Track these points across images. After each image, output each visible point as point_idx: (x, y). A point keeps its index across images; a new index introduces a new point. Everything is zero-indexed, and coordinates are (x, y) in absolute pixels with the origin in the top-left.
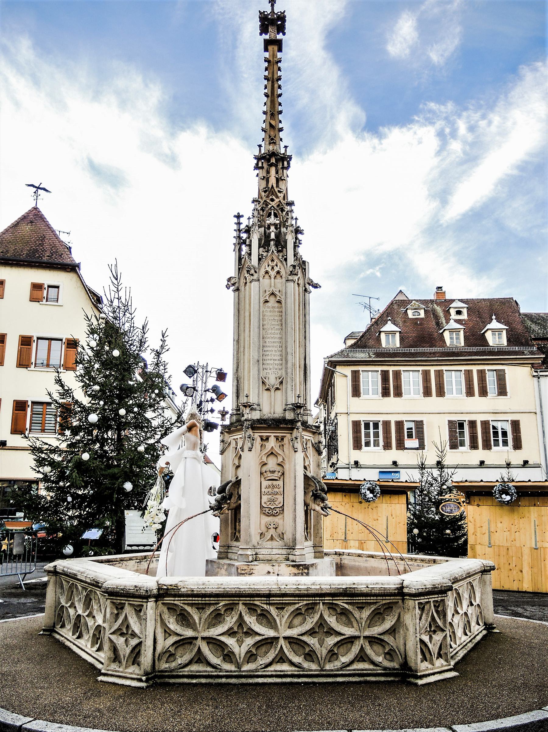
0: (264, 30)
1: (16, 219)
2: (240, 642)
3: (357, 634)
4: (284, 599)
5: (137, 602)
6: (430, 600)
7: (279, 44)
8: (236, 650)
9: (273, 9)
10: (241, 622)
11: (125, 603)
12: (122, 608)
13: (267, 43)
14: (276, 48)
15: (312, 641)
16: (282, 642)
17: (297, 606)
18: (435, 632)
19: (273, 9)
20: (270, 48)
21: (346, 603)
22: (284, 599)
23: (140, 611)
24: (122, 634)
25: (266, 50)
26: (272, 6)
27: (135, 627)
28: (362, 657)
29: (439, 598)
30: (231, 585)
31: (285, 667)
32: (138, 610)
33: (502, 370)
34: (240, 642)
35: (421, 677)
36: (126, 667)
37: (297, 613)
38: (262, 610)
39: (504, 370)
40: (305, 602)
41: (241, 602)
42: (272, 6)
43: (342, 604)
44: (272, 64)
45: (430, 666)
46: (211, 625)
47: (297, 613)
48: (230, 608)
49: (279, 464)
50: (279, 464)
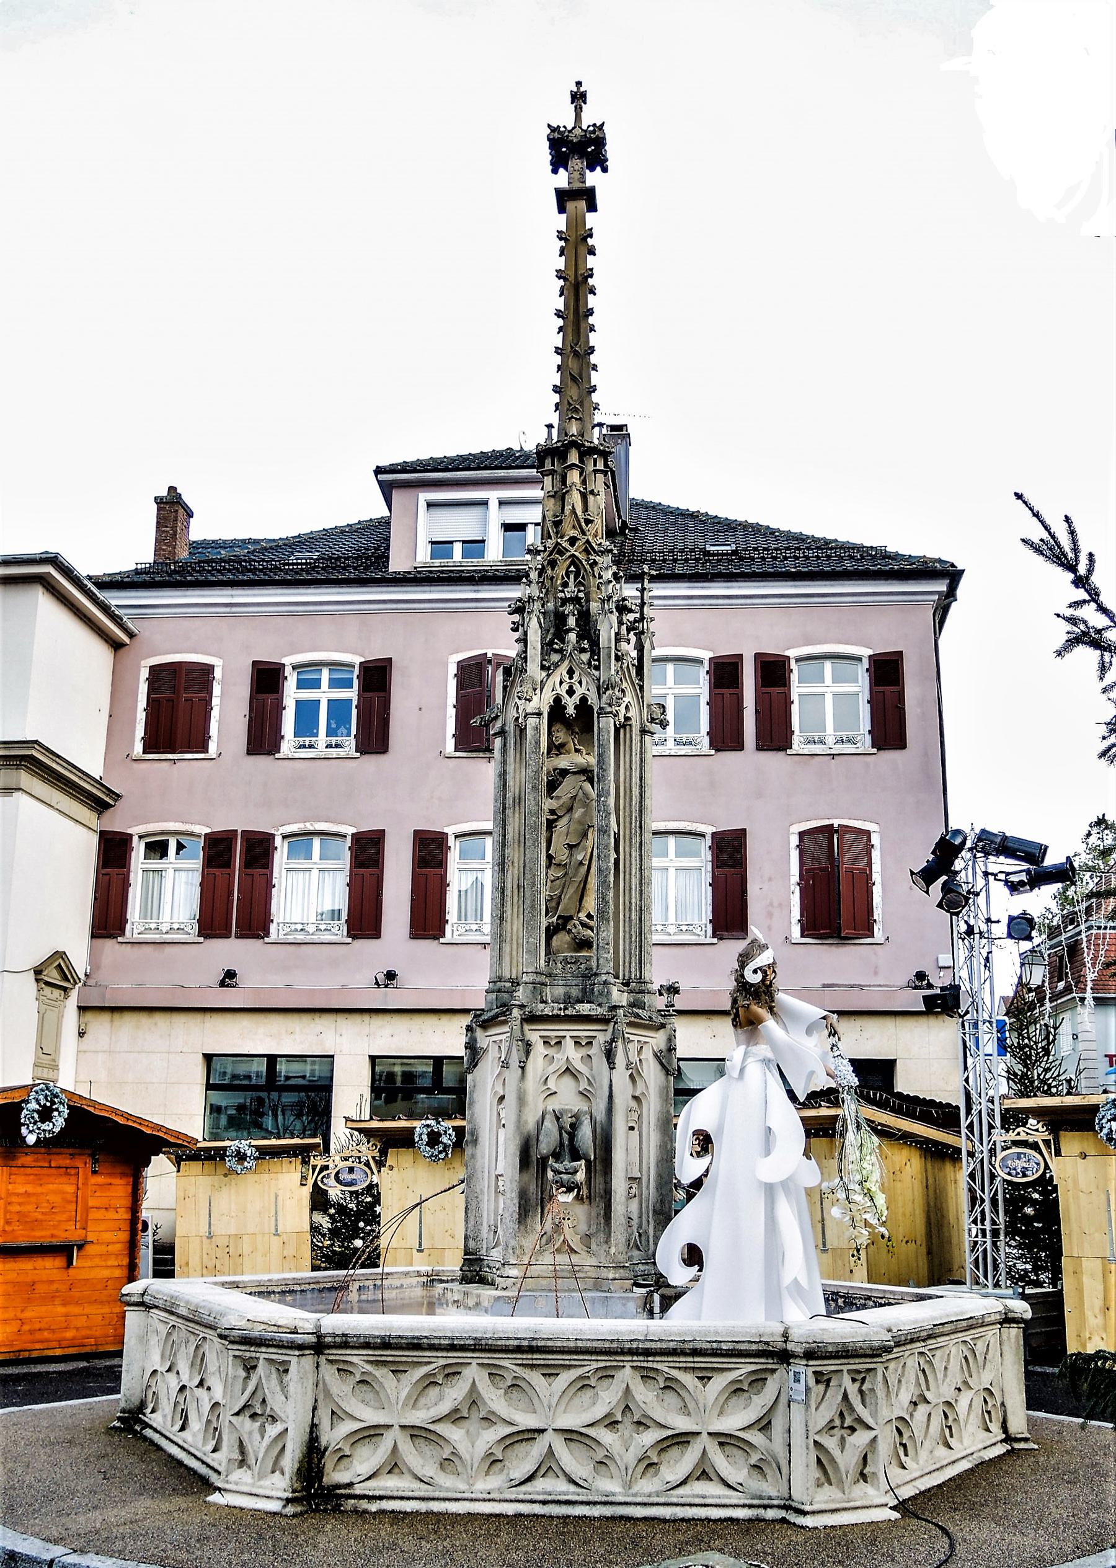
0: (558, 163)
1: (674, 505)
2: (472, 1438)
3: (694, 1428)
4: (535, 1356)
5: (278, 1355)
6: (258, 1355)
7: (589, 197)
8: (463, 1448)
9: (578, 118)
10: (474, 1400)
11: (258, 1359)
12: (254, 1367)
13: (563, 197)
14: (583, 204)
15: (605, 1436)
16: (704, 1440)
17: (579, 1372)
18: (853, 1430)
19: (578, 118)
20: (570, 206)
21: (368, 1362)
22: (535, 1356)
23: (286, 1371)
24: (254, 1416)
25: (562, 209)
26: (578, 111)
27: (276, 1402)
28: (548, 1466)
29: (248, 1354)
30: (737, 1336)
31: (711, 1490)
32: (283, 1369)
33: (808, 936)
34: (472, 1438)
35: (804, 1513)
36: (261, 1476)
37: (736, 1390)
38: (667, 1379)
39: (802, 936)
40: (595, 1365)
41: (628, 1365)
42: (578, 111)
43: (666, 1370)
44: (576, 244)
45: (840, 1495)
46: (414, 1401)
47: (736, 1390)
48: (606, 1375)
49: (635, 1098)
50: (635, 1098)
